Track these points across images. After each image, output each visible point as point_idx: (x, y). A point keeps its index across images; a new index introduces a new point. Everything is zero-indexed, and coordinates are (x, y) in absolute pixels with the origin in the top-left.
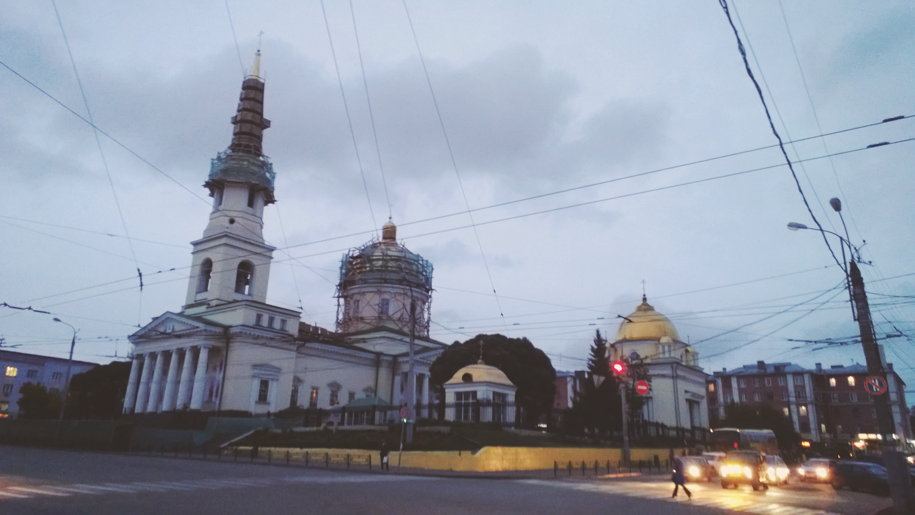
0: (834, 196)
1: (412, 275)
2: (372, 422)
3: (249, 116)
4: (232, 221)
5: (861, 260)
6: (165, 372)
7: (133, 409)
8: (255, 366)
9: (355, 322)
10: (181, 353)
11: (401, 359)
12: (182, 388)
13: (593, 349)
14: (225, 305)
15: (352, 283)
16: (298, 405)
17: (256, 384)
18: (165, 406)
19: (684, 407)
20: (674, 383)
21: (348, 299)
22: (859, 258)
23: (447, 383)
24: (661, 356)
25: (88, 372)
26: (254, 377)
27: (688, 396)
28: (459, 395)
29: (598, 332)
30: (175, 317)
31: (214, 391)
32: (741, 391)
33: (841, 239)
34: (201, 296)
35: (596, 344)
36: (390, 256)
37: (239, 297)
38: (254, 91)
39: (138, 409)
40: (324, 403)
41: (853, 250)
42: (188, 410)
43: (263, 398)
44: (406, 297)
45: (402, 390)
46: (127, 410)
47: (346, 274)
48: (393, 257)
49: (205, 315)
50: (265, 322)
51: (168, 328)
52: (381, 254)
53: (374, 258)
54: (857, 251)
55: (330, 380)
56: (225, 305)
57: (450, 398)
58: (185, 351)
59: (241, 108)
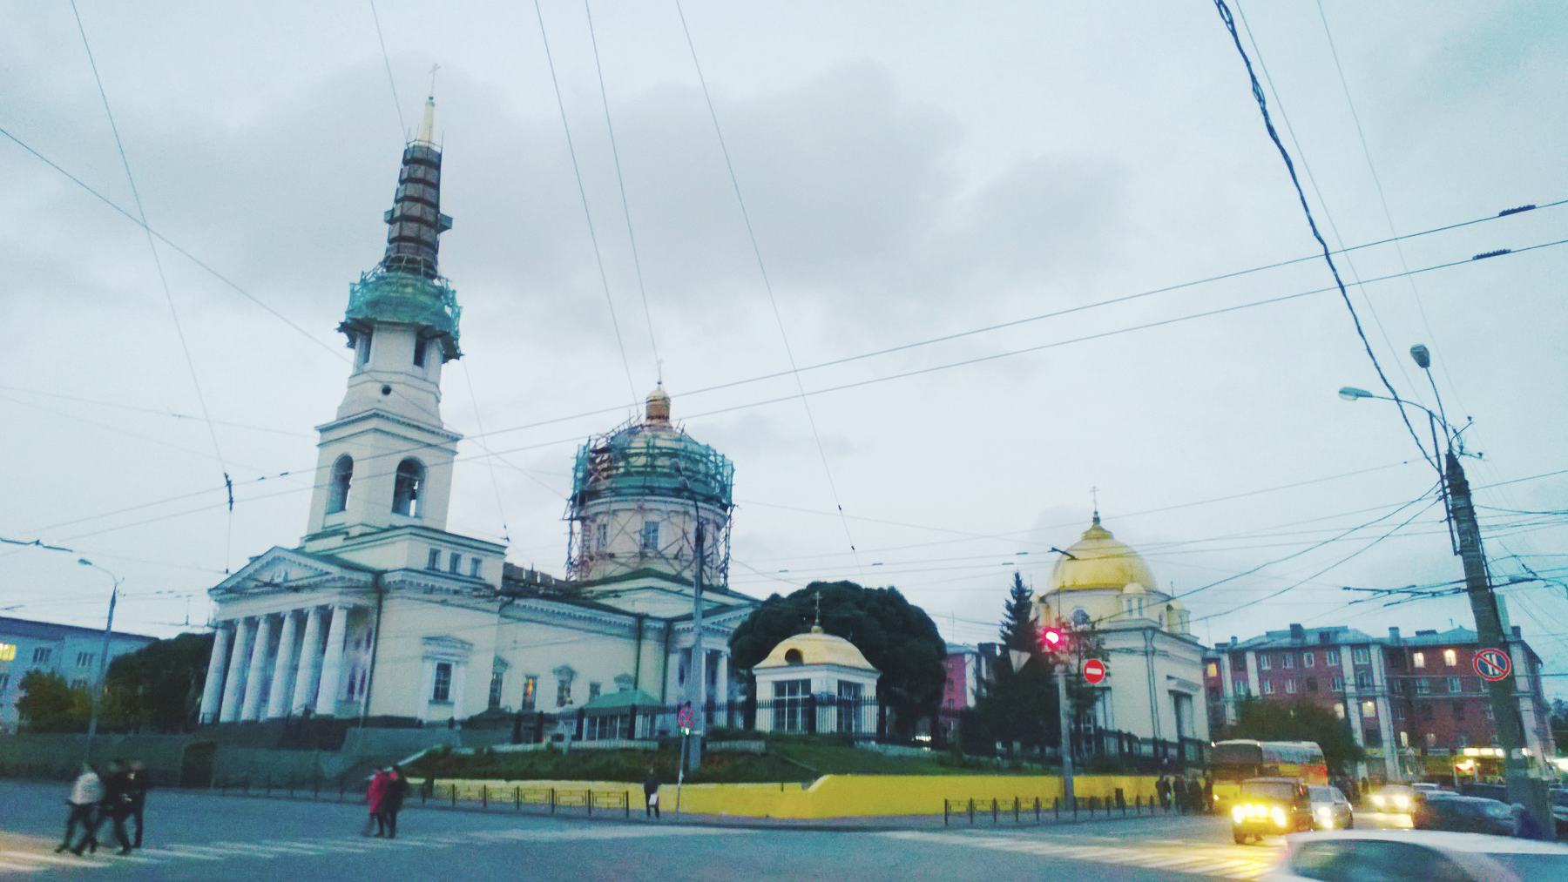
0: (1416, 342)
1: (696, 480)
4: (387, 391)
5: (1464, 451)
6: (272, 651)
8: (429, 639)
10: (300, 618)
11: (680, 626)
15: (594, 494)
17: (430, 672)
18: (273, 710)
19: (1166, 704)
21: (588, 522)
24: (1126, 616)
25: (140, 653)
26: (425, 658)
27: (1172, 685)
28: (780, 687)
29: (1017, 576)
31: (357, 684)
35: (1014, 597)
37: (398, 520)
39: (225, 717)
40: (546, 703)
41: (1451, 434)
42: (312, 716)
43: (441, 695)
44: (687, 517)
45: (682, 678)
46: (206, 717)
47: (584, 480)
49: (341, 552)
53: (632, 451)
54: (1457, 434)
55: (559, 664)
57: (765, 692)
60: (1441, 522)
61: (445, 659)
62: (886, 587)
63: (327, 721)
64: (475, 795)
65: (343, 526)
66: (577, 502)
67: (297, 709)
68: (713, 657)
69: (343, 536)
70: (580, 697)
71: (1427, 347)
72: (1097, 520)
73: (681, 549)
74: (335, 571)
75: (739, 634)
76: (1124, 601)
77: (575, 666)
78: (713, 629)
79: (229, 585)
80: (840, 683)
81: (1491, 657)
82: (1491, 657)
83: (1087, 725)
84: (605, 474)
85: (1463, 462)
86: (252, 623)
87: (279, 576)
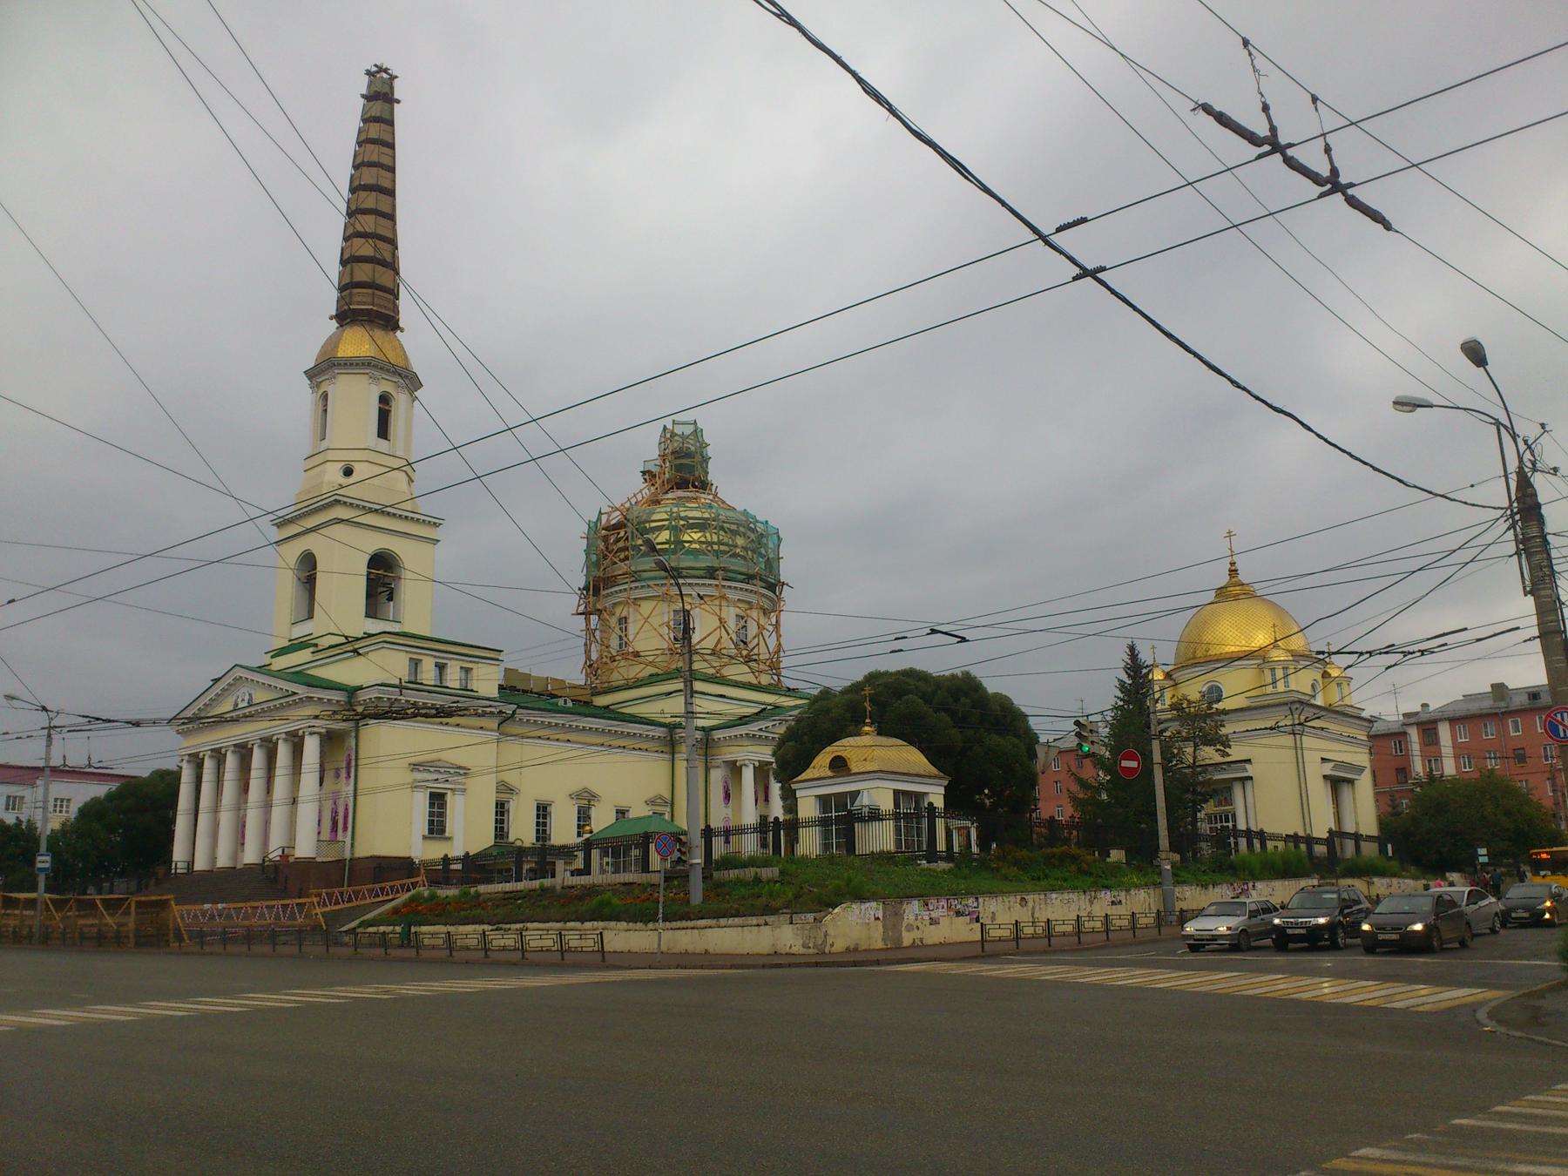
0: (1466, 336)
1: (735, 555)
2: (645, 866)
3: (366, 249)
4: (348, 472)
5: (1539, 465)
6: (244, 788)
7: (191, 863)
8: (415, 767)
9: (623, 663)
10: (244, 752)
11: (717, 735)
12: (279, 814)
13: (1122, 683)
14: (352, 647)
15: (610, 581)
16: (511, 839)
17: (421, 801)
18: (250, 856)
19: (1320, 795)
20: (404, 785)
21: (605, 615)
22: (1534, 464)
23: (803, 776)
24: (1270, 689)
25: (110, 797)
26: (415, 786)
27: (1328, 769)
28: (824, 801)
29: (1132, 648)
30: (250, 675)
31: (339, 821)
32: (1459, 752)
33: (1498, 424)
34: (300, 631)
35: (1129, 676)
36: (686, 518)
37: (374, 626)
38: (374, 193)
39: (200, 865)
40: (563, 832)
41: (1522, 447)
42: (291, 860)
43: (437, 828)
44: (724, 603)
45: (727, 796)
46: (179, 865)
47: (597, 564)
48: (691, 521)
49: (308, 669)
50: (428, 674)
51: (239, 700)
52: (665, 516)
53: (653, 525)
54: (1529, 447)
55: (575, 786)
56: (352, 647)
57: (808, 808)
58: (251, 750)
59: (350, 231)
60: (1510, 556)
61: (440, 787)
62: (958, 672)
63: (308, 865)
64: (473, 942)
65: (312, 637)
66: (591, 592)
67: (275, 855)
68: (761, 771)
69: (312, 649)
70: (602, 819)
71: (1480, 340)
72: (1233, 572)
73: (719, 642)
74: (302, 691)
75: (783, 741)
76: (1268, 673)
77: (595, 789)
78: (760, 736)
79: (188, 713)
80: (897, 793)
81: (1562, 716)
82: (1562, 716)
83: (1225, 824)
84: (622, 555)
85: (1538, 480)
86: (219, 756)
87: (243, 700)
